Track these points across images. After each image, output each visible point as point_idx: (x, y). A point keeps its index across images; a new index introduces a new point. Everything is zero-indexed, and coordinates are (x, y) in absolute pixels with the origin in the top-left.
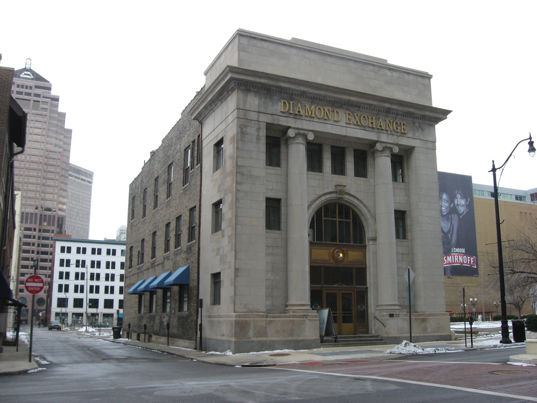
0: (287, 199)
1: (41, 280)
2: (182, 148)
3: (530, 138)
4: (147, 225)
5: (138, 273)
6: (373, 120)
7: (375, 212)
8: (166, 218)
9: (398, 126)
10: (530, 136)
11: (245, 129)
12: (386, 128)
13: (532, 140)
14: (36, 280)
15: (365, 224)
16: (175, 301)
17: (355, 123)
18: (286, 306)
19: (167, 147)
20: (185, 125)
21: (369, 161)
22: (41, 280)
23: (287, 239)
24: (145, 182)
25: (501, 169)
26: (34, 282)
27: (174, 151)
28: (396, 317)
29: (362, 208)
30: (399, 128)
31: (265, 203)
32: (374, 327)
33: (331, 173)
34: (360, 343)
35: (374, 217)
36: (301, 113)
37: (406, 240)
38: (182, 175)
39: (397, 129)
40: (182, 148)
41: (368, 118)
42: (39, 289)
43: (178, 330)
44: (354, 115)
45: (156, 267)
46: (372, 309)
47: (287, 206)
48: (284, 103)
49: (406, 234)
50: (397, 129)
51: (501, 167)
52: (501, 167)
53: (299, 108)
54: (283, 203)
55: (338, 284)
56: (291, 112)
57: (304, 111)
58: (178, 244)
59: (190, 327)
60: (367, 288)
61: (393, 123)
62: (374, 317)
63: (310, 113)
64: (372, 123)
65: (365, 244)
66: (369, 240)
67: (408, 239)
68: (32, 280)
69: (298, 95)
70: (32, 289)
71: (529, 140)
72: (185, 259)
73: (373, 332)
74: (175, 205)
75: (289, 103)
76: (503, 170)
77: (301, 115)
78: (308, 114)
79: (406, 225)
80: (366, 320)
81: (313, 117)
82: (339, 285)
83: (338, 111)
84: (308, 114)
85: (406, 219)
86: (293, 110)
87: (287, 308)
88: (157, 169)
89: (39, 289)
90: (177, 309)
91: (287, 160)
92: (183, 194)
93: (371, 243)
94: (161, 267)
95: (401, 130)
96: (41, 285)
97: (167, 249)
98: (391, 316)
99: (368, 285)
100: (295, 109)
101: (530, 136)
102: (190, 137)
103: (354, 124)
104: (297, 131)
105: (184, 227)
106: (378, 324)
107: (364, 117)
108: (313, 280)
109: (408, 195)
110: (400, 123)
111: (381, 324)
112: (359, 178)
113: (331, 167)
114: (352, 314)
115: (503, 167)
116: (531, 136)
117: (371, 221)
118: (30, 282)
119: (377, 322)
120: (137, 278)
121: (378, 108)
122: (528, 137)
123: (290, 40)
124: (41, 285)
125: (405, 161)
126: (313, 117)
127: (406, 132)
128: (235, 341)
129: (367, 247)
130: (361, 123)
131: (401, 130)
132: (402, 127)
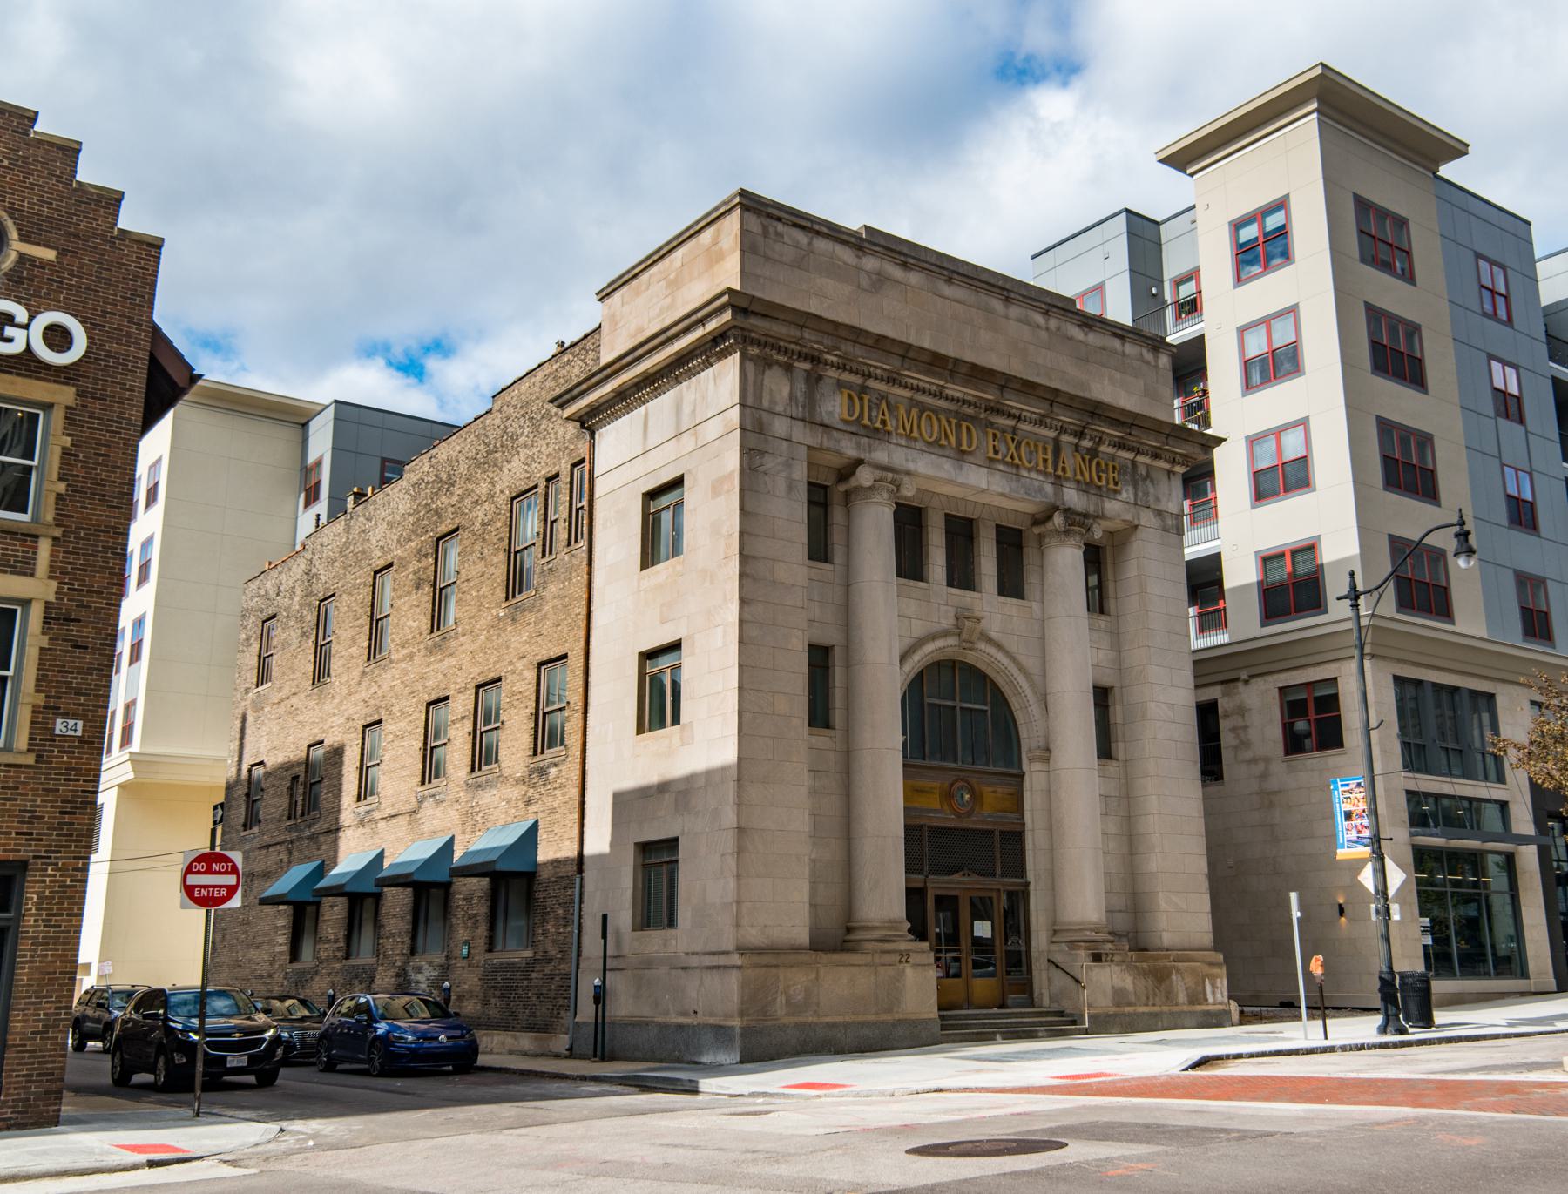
0: (847, 647)
1: (230, 864)
2: (502, 492)
3: (1462, 523)
4: (336, 701)
5: (292, 842)
6: (1046, 454)
7: (1045, 687)
8: (430, 683)
9: (1103, 471)
10: (1461, 517)
11: (757, 460)
12: (1075, 475)
13: (1466, 528)
14: (215, 867)
15: (1020, 718)
16: (469, 923)
17: (1008, 459)
18: (849, 930)
19: (428, 483)
20: (511, 429)
21: (1030, 555)
22: (230, 864)
23: (848, 752)
24: (323, 578)
25: (1376, 594)
26: (209, 871)
27: (461, 499)
28: (1106, 961)
29: (1015, 675)
30: (1104, 475)
31: (807, 654)
32: (1045, 983)
33: (945, 583)
34: (977, 1033)
35: (1044, 700)
36: (889, 428)
37: (1114, 763)
38: (504, 568)
39: (1099, 478)
40: (502, 492)
41: (1036, 446)
42: (224, 892)
43: (486, 1002)
44: (1005, 437)
45: (382, 824)
46: (1040, 939)
47: (848, 666)
48: (850, 397)
49: (1113, 745)
50: (1099, 478)
51: (1376, 589)
52: (1376, 589)
53: (883, 414)
54: (838, 657)
55: (962, 873)
56: (866, 421)
57: (894, 422)
58: (483, 755)
59: (539, 995)
60: (1027, 884)
61: (1090, 461)
62: (1049, 961)
63: (908, 428)
64: (1045, 461)
65: (1020, 766)
66: (1031, 760)
67: (1117, 760)
68: (203, 866)
69: (882, 380)
70: (204, 893)
71: (1457, 529)
72: (517, 800)
73: (1046, 1001)
74: (469, 647)
75: (861, 399)
76: (1381, 595)
77: (889, 433)
78: (904, 429)
79: (1112, 721)
80: (1024, 969)
81: (915, 440)
82: (964, 875)
83: (972, 427)
84: (904, 429)
85: (1111, 709)
86: (870, 419)
87: (852, 937)
88: (381, 543)
89: (224, 892)
90: (481, 943)
91: (848, 546)
92: (509, 621)
93: (1037, 766)
94: (405, 823)
95: (1108, 483)
96: (231, 880)
97: (430, 770)
98: (1097, 958)
99: (1030, 876)
100: (874, 413)
101: (1461, 517)
102: (534, 465)
103: (1006, 463)
104: (878, 473)
105: (512, 711)
106: (1060, 980)
107: (1028, 444)
108: (913, 865)
109: (1117, 646)
110: (1106, 465)
111: (1070, 980)
112: (1009, 600)
113: (945, 569)
114: (993, 952)
115: (1381, 590)
116: (1464, 518)
117: (1035, 710)
118: (199, 872)
119: (1057, 974)
120: (284, 857)
121: (1060, 424)
122: (1455, 520)
123: (855, 229)
124: (231, 880)
125: (1109, 559)
126: (915, 440)
127: (1118, 488)
128: (741, 1028)
129: (1027, 778)
130: (1020, 459)
131: (1108, 483)
132: (1111, 475)
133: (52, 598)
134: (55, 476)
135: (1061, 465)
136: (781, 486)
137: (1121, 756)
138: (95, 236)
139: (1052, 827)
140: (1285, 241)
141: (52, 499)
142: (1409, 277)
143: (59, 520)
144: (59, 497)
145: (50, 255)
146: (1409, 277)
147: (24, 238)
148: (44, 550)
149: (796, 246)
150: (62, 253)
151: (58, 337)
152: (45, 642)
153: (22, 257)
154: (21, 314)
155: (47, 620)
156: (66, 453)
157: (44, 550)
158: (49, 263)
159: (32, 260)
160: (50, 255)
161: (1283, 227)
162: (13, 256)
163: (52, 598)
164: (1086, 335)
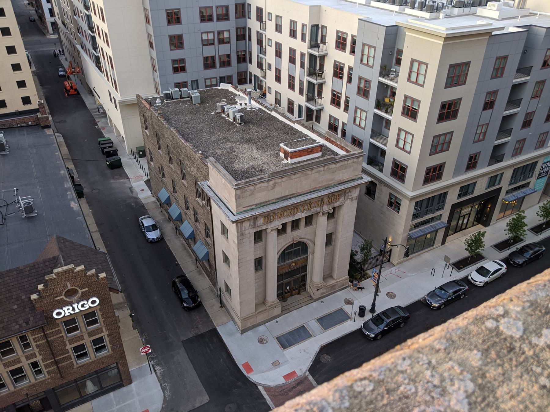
26: (145, 349)
124: (149, 348)
133: (108, 334)
134: (101, 319)
135: (323, 203)
136: (248, 242)
137: (333, 244)
138: (93, 282)
139: (312, 264)
140: (306, 256)
141: (102, 322)
142: (468, 64)
143: (104, 324)
144: (103, 321)
145: (87, 289)
146: (468, 64)
147: (81, 289)
148: (104, 329)
149: (251, 190)
150: (88, 288)
151: (93, 302)
152: (109, 339)
153: (82, 292)
154: (86, 302)
155: (108, 337)
156: (101, 315)
157: (104, 329)
158: (87, 291)
159: (84, 292)
160: (87, 289)
161: (334, 119)
162: (80, 293)
163: (108, 334)
164: (336, 165)
